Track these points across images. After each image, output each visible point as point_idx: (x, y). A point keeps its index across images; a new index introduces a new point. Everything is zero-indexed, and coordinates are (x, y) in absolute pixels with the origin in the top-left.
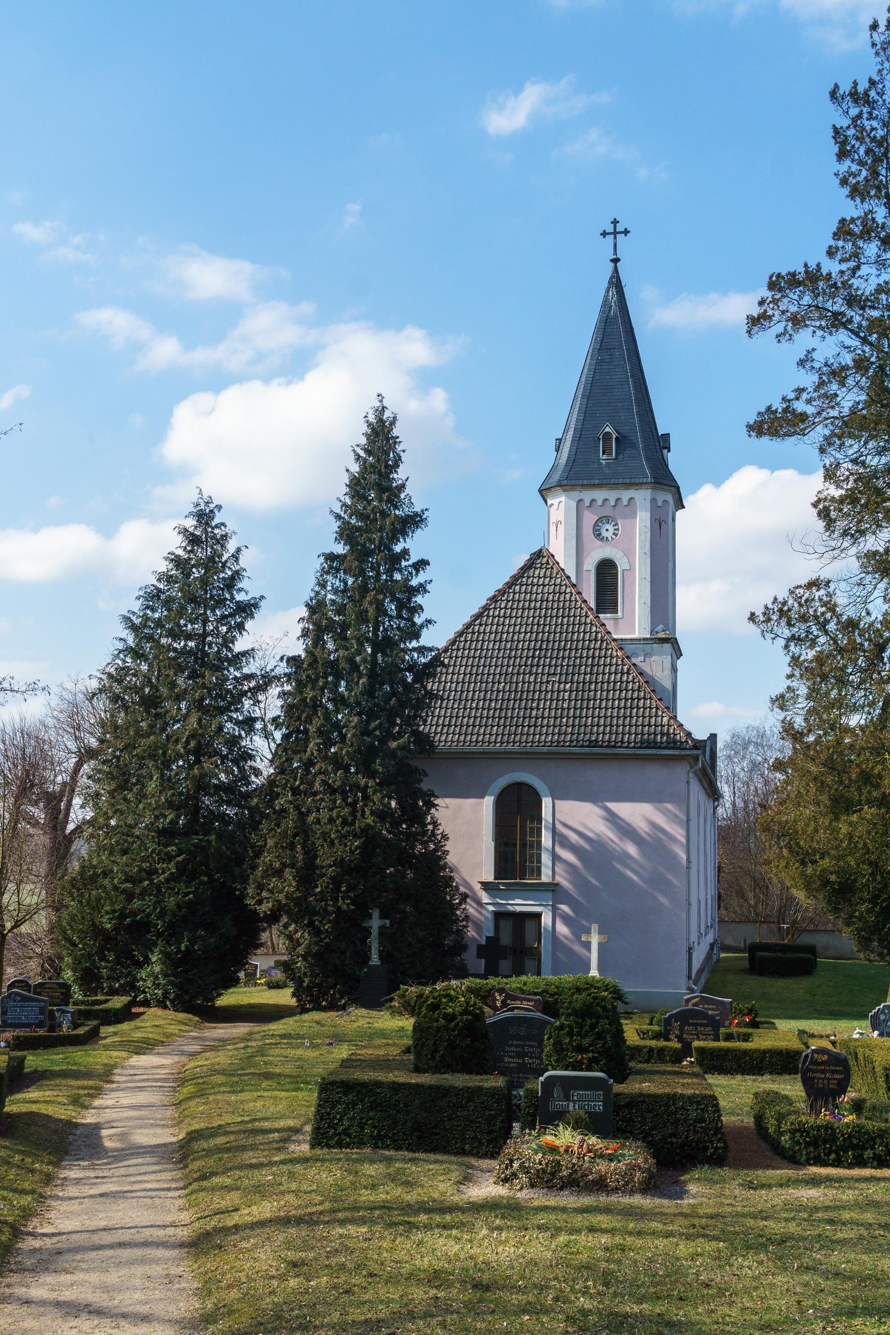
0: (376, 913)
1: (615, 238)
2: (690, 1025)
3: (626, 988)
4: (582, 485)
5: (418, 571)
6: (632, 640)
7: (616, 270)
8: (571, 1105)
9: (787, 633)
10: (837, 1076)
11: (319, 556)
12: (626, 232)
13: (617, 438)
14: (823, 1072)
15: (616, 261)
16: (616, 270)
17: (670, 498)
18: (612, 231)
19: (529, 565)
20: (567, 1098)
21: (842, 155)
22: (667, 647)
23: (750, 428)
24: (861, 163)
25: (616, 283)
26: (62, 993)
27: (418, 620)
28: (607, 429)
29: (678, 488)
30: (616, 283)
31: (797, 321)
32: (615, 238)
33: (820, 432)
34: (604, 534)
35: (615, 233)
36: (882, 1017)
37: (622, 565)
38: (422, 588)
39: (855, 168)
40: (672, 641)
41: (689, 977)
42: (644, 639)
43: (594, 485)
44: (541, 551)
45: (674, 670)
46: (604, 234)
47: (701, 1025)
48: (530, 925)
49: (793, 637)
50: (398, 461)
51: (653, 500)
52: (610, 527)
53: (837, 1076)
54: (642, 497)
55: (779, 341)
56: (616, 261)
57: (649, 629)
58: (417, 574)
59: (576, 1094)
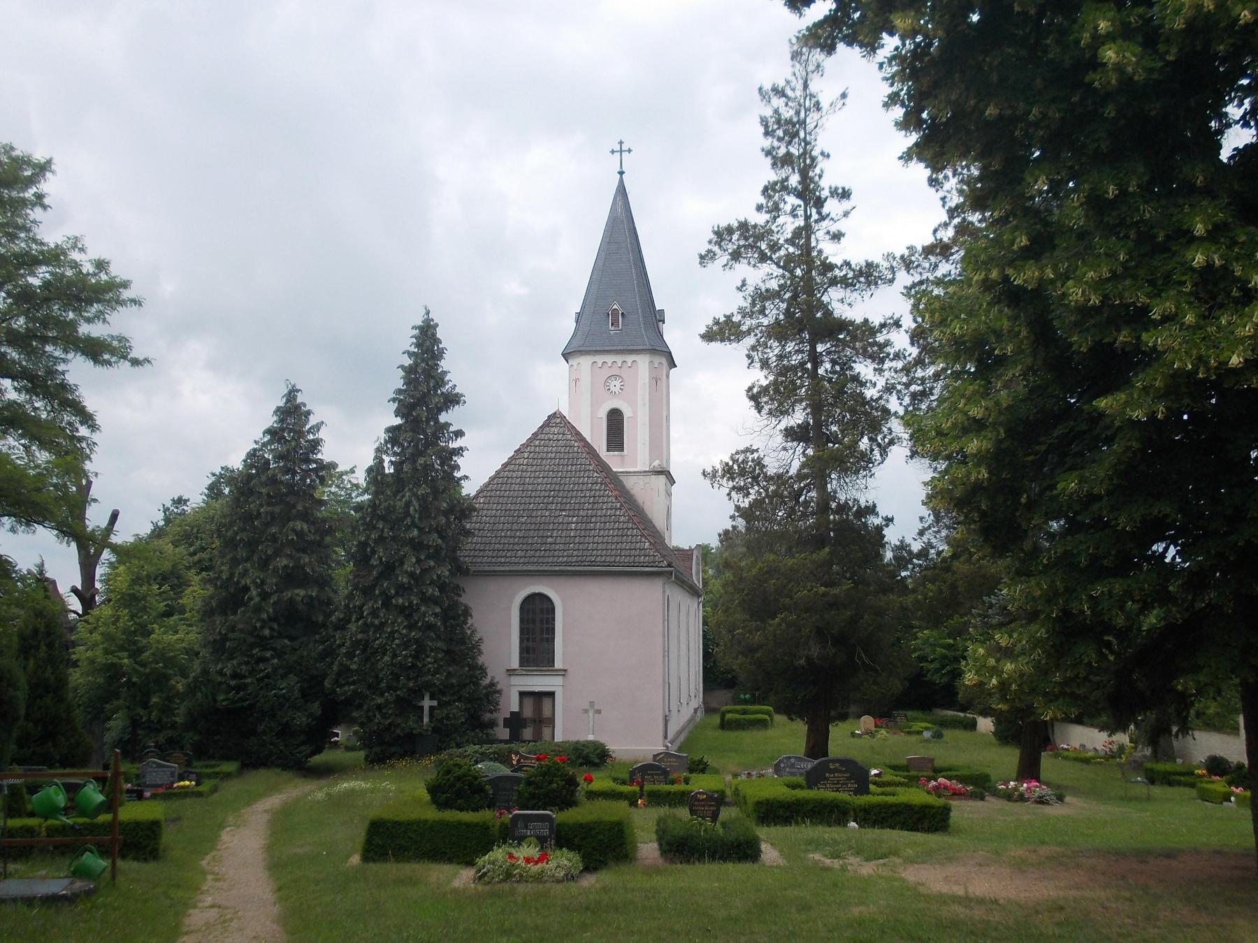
0: (427, 697)
1: (621, 155)
2: (649, 775)
3: (611, 747)
4: (596, 351)
5: (457, 437)
6: (634, 472)
7: (621, 181)
8: (529, 831)
9: (731, 484)
10: (712, 808)
11: (404, 353)
12: (629, 151)
13: (622, 313)
14: (703, 806)
15: (621, 173)
16: (621, 181)
17: (664, 361)
18: (619, 149)
19: (547, 424)
20: (527, 828)
21: (767, 133)
22: (662, 478)
23: (897, 124)
24: (780, 139)
25: (622, 191)
26: (186, 761)
27: (457, 474)
28: (615, 307)
29: (670, 353)
30: (622, 191)
31: (736, 256)
32: (621, 155)
33: (750, 341)
34: (612, 389)
35: (621, 151)
36: (782, 765)
37: (627, 413)
38: (459, 451)
39: (776, 144)
40: (665, 473)
41: (666, 737)
42: (645, 472)
43: (604, 351)
44: (555, 413)
45: (669, 495)
46: (621, 143)
47: (656, 775)
48: (546, 703)
49: (734, 488)
50: (442, 352)
51: (651, 362)
52: (618, 383)
53: (712, 808)
54: (643, 364)
55: (724, 270)
56: (621, 173)
57: (648, 463)
58: (456, 440)
59: (532, 825)
